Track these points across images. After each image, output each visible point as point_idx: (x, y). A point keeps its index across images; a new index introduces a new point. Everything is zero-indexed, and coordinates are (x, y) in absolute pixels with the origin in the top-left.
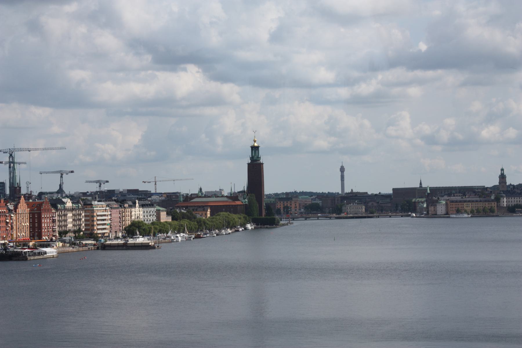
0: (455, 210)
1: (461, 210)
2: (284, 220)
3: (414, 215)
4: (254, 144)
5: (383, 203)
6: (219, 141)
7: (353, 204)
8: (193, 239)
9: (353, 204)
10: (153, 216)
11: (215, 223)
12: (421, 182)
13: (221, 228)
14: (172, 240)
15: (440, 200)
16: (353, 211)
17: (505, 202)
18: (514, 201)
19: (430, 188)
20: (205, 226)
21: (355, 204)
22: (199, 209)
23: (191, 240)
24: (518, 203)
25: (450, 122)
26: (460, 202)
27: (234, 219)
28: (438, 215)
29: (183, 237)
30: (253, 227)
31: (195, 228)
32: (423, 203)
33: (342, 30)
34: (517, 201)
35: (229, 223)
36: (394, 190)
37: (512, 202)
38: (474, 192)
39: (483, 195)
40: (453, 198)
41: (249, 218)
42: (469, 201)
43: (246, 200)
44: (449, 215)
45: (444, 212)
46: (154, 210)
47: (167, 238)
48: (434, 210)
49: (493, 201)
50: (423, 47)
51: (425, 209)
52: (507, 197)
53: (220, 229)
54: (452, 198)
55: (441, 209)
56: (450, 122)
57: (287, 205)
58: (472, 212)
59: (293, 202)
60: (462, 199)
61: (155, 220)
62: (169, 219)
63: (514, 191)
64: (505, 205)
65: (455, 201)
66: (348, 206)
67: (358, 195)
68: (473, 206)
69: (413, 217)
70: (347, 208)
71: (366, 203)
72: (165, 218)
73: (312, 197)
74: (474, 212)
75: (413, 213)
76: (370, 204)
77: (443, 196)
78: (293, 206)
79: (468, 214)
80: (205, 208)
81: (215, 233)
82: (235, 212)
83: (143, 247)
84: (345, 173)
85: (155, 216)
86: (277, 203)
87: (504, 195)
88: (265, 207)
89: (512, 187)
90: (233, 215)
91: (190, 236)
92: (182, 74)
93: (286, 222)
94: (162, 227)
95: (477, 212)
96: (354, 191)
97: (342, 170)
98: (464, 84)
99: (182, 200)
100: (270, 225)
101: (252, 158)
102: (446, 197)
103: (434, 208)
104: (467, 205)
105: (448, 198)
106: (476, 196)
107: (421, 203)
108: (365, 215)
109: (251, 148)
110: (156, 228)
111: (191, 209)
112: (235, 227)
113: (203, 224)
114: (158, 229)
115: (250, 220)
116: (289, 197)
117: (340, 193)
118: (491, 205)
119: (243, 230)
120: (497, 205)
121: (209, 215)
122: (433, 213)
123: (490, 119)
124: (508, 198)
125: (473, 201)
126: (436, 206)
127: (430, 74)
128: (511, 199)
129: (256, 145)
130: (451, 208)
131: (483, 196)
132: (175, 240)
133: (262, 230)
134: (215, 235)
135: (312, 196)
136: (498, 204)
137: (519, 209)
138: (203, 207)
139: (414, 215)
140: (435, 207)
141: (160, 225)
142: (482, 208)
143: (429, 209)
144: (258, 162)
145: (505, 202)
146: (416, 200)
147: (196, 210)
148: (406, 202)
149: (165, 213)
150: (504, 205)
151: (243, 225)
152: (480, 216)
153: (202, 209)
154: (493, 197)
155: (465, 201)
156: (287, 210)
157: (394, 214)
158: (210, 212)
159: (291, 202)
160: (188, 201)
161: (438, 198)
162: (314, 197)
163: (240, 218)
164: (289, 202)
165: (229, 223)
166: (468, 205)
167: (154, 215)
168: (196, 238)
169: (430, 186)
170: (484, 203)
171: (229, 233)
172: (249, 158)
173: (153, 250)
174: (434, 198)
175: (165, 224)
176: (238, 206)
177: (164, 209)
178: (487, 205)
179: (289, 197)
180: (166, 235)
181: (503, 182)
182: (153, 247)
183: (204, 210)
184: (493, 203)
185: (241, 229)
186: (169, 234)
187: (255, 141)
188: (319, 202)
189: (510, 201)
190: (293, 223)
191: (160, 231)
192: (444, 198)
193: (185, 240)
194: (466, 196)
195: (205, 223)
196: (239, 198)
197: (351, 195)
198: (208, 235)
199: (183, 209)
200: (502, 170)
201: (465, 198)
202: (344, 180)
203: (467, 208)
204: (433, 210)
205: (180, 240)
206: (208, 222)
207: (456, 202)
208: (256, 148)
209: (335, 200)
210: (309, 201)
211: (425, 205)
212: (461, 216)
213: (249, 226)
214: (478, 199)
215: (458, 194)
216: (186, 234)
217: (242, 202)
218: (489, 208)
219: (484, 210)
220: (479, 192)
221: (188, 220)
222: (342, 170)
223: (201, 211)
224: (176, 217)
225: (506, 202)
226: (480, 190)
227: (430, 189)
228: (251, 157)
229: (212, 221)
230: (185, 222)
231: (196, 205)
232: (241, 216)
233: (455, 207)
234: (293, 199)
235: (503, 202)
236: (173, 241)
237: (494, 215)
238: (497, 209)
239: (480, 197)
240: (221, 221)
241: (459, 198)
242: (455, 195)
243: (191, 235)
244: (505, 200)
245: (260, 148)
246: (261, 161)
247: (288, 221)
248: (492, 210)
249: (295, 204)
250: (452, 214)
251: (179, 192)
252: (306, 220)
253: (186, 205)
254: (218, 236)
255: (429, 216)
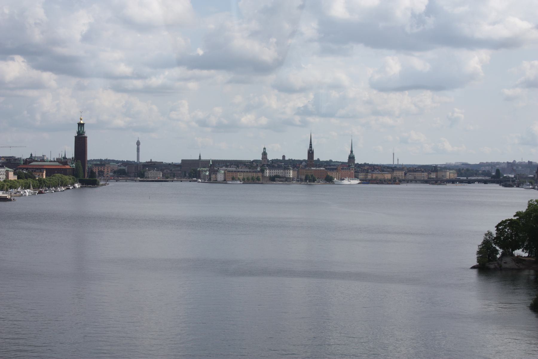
0: (231, 178)
1: (235, 178)
2: (103, 181)
3: (200, 181)
4: (80, 122)
5: (175, 171)
6: (38, 117)
7: (153, 171)
8: (37, 194)
9: (153, 171)
10: (3, 175)
11: (52, 182)
12: (200, 155)
13: (57, 186)
14: (22, 194)
15: (220, 170)
16: (153, 176)
17: (267, 173)
18: (275, 172)
19: (212, 160)
20: (45, 184)
21: (154, 171)
22: (37, 171)
23: (36, 195)
24: (277, 174)
25: (218, 110)
26: (235, 172)
27: (66, 179)
28: (218, 181)
29: (29, 192)
30: (79, 186)
31: (37, 185)
32: (206, 171)
33: (139, 35)
34: (276, 173)
35: (62, 182)
36: (182, 160)
37: (272, 173)
38: (245, 165)
39: (252, 167)
40: (229, 169)
41: (76, 179)
42: (242, 172)
43: (74, 165)
44: (226, 181)
45: (222, 179)
46: (4, 171)
47: (17, 193)
48: (215, 177)
49: (259, 172)
50: (200, 52)
51: (207, 176)
52: (269, 169)
53: (56, 187)
54: (229, 168)
55: (220, 176)
56: (218, 110)
57: (101, 169)
58: (244, 180)
59: (106, 167)
60: (236, 170)
61: (5, 178)
62: (16, 178)
63: (273, 165)
64: (268, 176)
65: (231, 171)
66: (150, 172)
67: (156, 164)
68: (244, 175)
69: (199, 182)
70: (149, 174)
71: (162, 170)
72: (12, 177)
73: (118, 164)
74: (245, 180)
75: (199, 179)
76: (165, 171)
77: (222, 167)
78: (106, 170)
79: (241, 182)
80: (42, 170)
81: (53, 190)
82: (66, 174)
83: (1, 199)
84: (140, 146)
85: (5, 175)
86: (93, 167)
87: (267, 168)
88: (87, 171)
89: (271, 162)
90: (66, 176)
91: (35, 192)
92: (10, 63)
93: (104, 183)
94: (12, 184)
95: (247, 180)
96: (152, 161)
97: (138, 143)
98: (230, 82)
99: (22, 163)
100: (92, 185)
101: (78, 133)
102: (224, 168)
103: (215, 176)
104: (240, 175)
105: (225, 169)
106: (247, 168)
107: (204, 172)
108: (162, 180)
109: (77, 124)
110: (7, 185)
111: (30, 170)
112: (67, 186)
113: (43, 183)
114: (9, 185)
115: (77, 181)
116: (102, 163)
117: (136, 161)
118: (257, 175)
119: (72, 188)
120: (262, 175)
121: (44, 177)
122: (215, 180)
123: (248, 109)
124: (270, 170)
125: (244, 172)
126: (217, 174)
127: (205, 72)
128: (273, 171)
129: (82, 122)
130: (228, 176)
131: (252, 168)
132: (24, 195)
133: (86, 188)
134: (54, 191)
135: (118, 163)
136: (263, 174)
137: (278, 179)
138: (40, 169)
139: (200, 181)
140: (216, 175)
141: (11, 183)
142: (251, 177)
143: (212, 176)
144: (83, 135)
145: (267, 173)
146: (200, 169)
147: (35, 171)
148: (192, 171)
149: (13, 173)
150: (267, 175)
151: (73, 184)
152: (250, 183)
153: (39, 171)
154: (259, 169)
155: (239, 172)
156: (101, 173)
157: (185, 179)
158: (46, 173)
159: (104, 167)
160: (27, 164)
161: (218, 168)
162: (120, 164)
163: (70, 179)
164: (103, 167)
165: (62, 182)
166: (241, 175)
167: (4, 174)
168: (39, 193)
169: (212, 159)
170: (253, 173)
171: (63, 191)
172: (76, 132)
173: (9, 202)
174: (216, 169)
175: (15, 181)
176: (68, 170)
177: (12, 170)
178: (255, 175)
179: (103, 163)
180: (17, 190)
181: (265, 158)
182: (10, 200)
183: (41, 172)
184: (259, 174)
185: (71, 188)
186: (19, 190)
187: (81, 119)
188: (126, 168)
189: (272, 173)
190: (109, 184)
191: (11, 187)
192: (223, 169)
193: (31, 195)
194: (239, 167)
195: (44, 182)
196: (68, 163)
197: (151, 164)
198: (48, 191)
199: (24, 170)
200: (265, 149)
201: (239, 169)
202: (139, 152)
203: (240, 177)
204: (214, 177)
205: (27, 195)
206: (46, 181)
207: (232, 172)
208: (82, 125)
209: (138, 167)
210: (116, 167)
211: (207, 173)
212: (235, 182)
213: (77, 185)
214: (248, 170)
215: (233, 166)
216: (32, 190)
217: (71, 166)
218: (256, 177)
219: (252, 179)
220: (248, 165)
221: (32, 179)
222: (138, 144)
223: (38, 172)
224: (21, 176)
225: (269, 173)
226: (249, 164)
227: (212, 161)
228: (77, 131)
229: (49, 180)
230: (30, 181)
231: (35, 167)
232: (71, 177)
233: (231, 176)
234: (106, 165)
235: (267, 173)
236: (22, 195)
237: (260, 182)
238: (262, 178)
239: (249, 169)
240: (56, 181)
241: (234, 169)
242: (231, 166)
243: (35, 191)
244: (268, 171)
245: (85, 124)
246: (86, 135)
247: (105, 183)
248: (258, 179)
249: (107, 169)
250: (228, 181)
251: (14, 156)
252: (117, 182)
253: (27, 167)
254: (56, 193)
255: (211, 182)
